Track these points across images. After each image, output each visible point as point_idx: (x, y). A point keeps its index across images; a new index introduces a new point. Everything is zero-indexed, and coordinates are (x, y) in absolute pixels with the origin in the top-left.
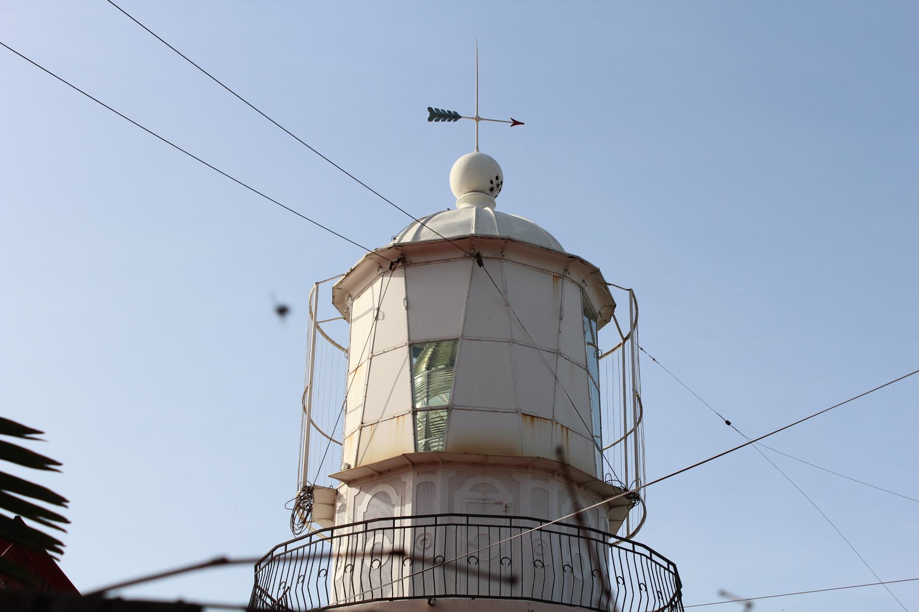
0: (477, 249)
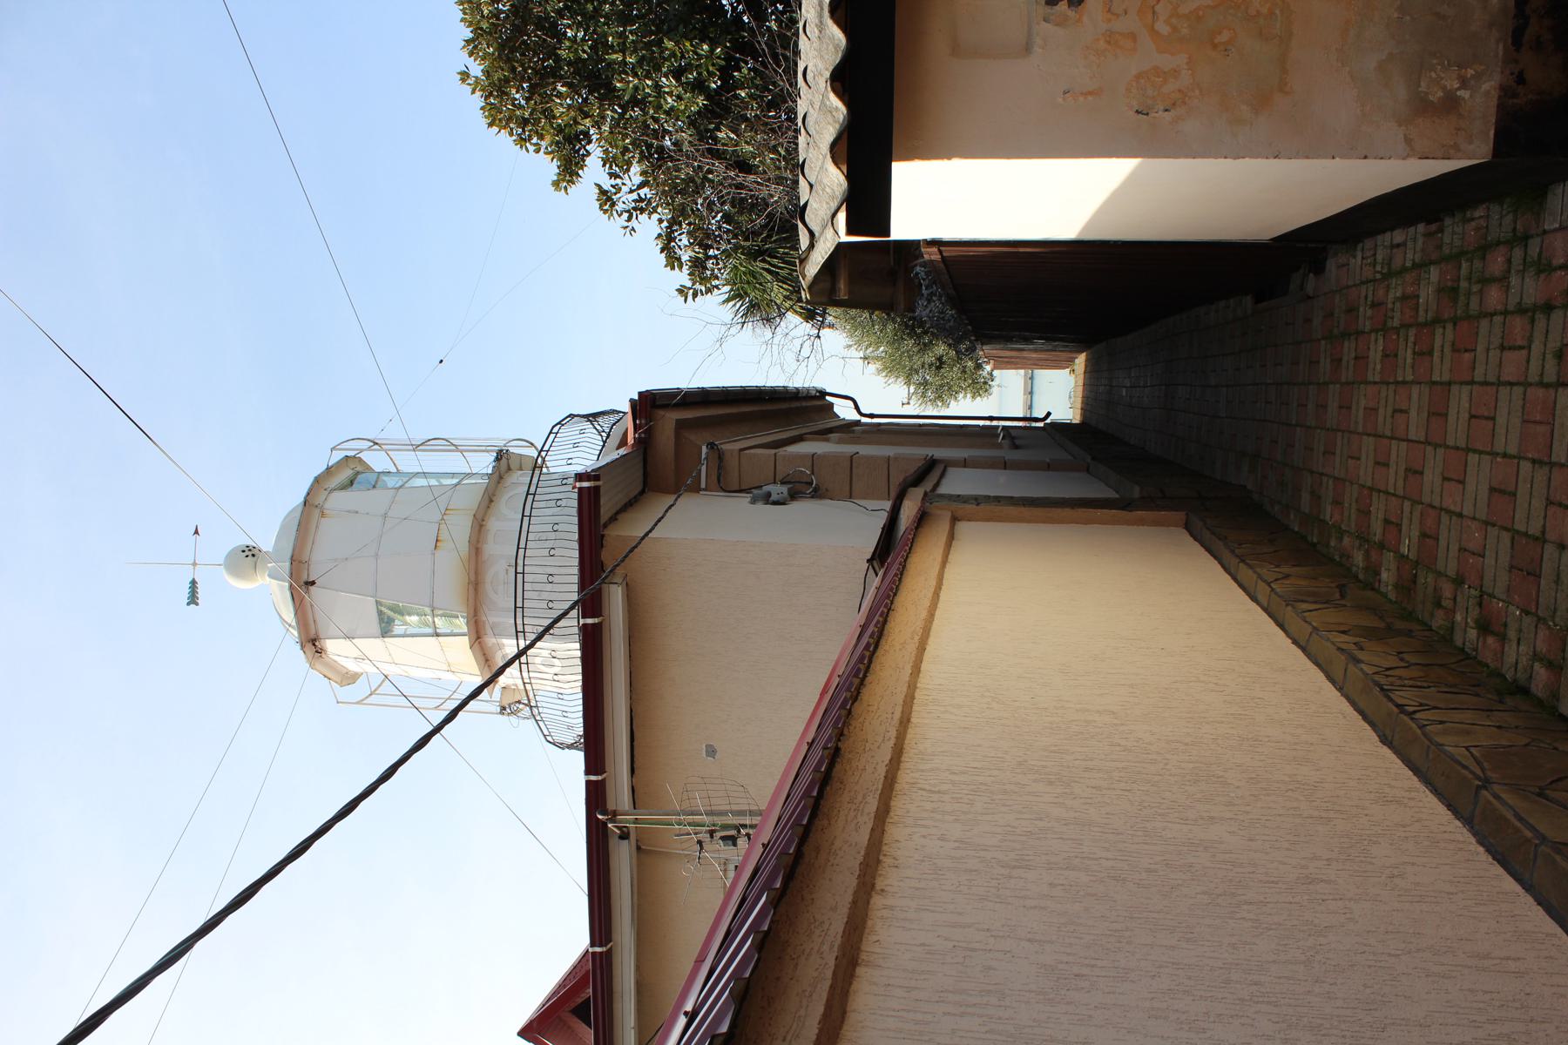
0: (302, 585)
